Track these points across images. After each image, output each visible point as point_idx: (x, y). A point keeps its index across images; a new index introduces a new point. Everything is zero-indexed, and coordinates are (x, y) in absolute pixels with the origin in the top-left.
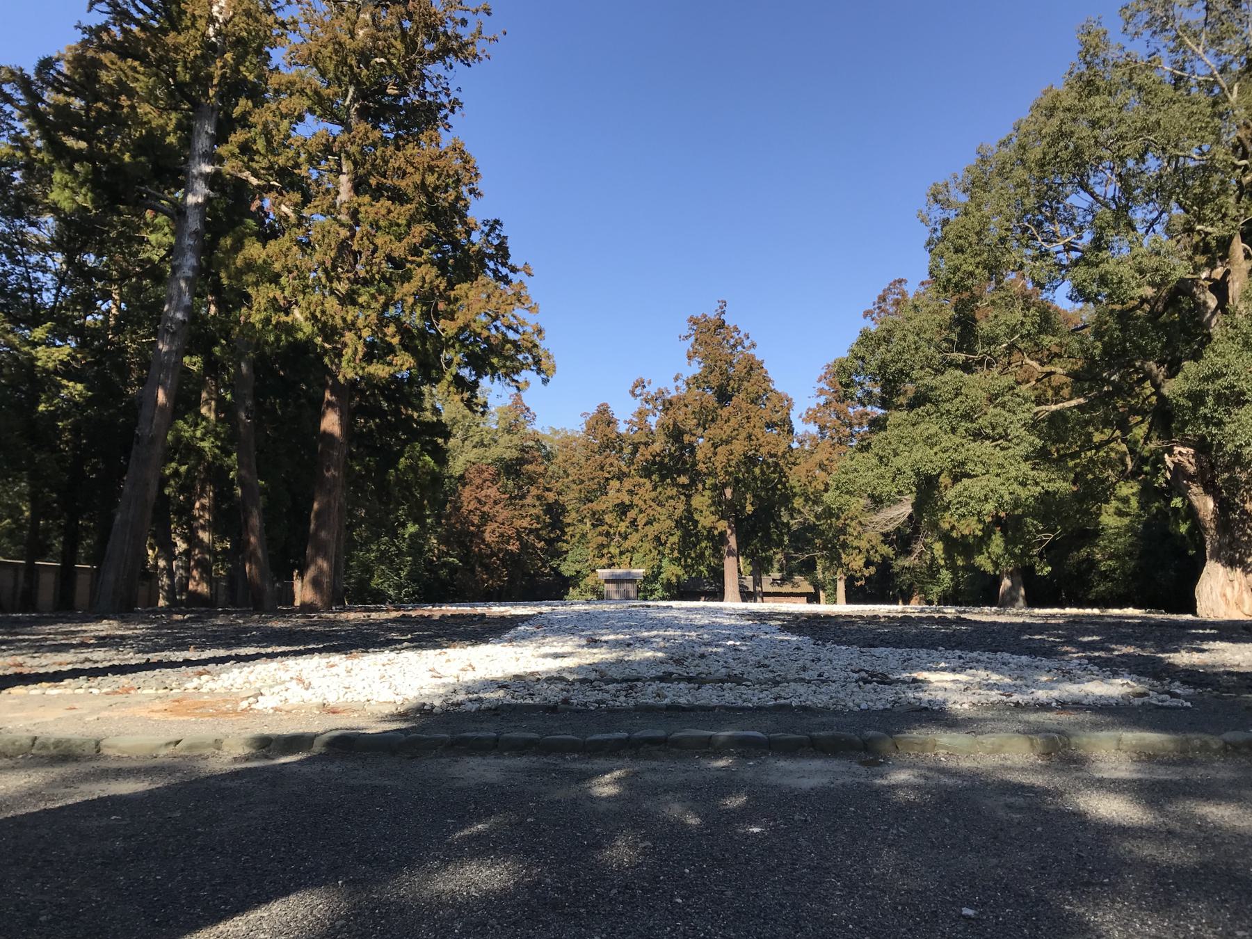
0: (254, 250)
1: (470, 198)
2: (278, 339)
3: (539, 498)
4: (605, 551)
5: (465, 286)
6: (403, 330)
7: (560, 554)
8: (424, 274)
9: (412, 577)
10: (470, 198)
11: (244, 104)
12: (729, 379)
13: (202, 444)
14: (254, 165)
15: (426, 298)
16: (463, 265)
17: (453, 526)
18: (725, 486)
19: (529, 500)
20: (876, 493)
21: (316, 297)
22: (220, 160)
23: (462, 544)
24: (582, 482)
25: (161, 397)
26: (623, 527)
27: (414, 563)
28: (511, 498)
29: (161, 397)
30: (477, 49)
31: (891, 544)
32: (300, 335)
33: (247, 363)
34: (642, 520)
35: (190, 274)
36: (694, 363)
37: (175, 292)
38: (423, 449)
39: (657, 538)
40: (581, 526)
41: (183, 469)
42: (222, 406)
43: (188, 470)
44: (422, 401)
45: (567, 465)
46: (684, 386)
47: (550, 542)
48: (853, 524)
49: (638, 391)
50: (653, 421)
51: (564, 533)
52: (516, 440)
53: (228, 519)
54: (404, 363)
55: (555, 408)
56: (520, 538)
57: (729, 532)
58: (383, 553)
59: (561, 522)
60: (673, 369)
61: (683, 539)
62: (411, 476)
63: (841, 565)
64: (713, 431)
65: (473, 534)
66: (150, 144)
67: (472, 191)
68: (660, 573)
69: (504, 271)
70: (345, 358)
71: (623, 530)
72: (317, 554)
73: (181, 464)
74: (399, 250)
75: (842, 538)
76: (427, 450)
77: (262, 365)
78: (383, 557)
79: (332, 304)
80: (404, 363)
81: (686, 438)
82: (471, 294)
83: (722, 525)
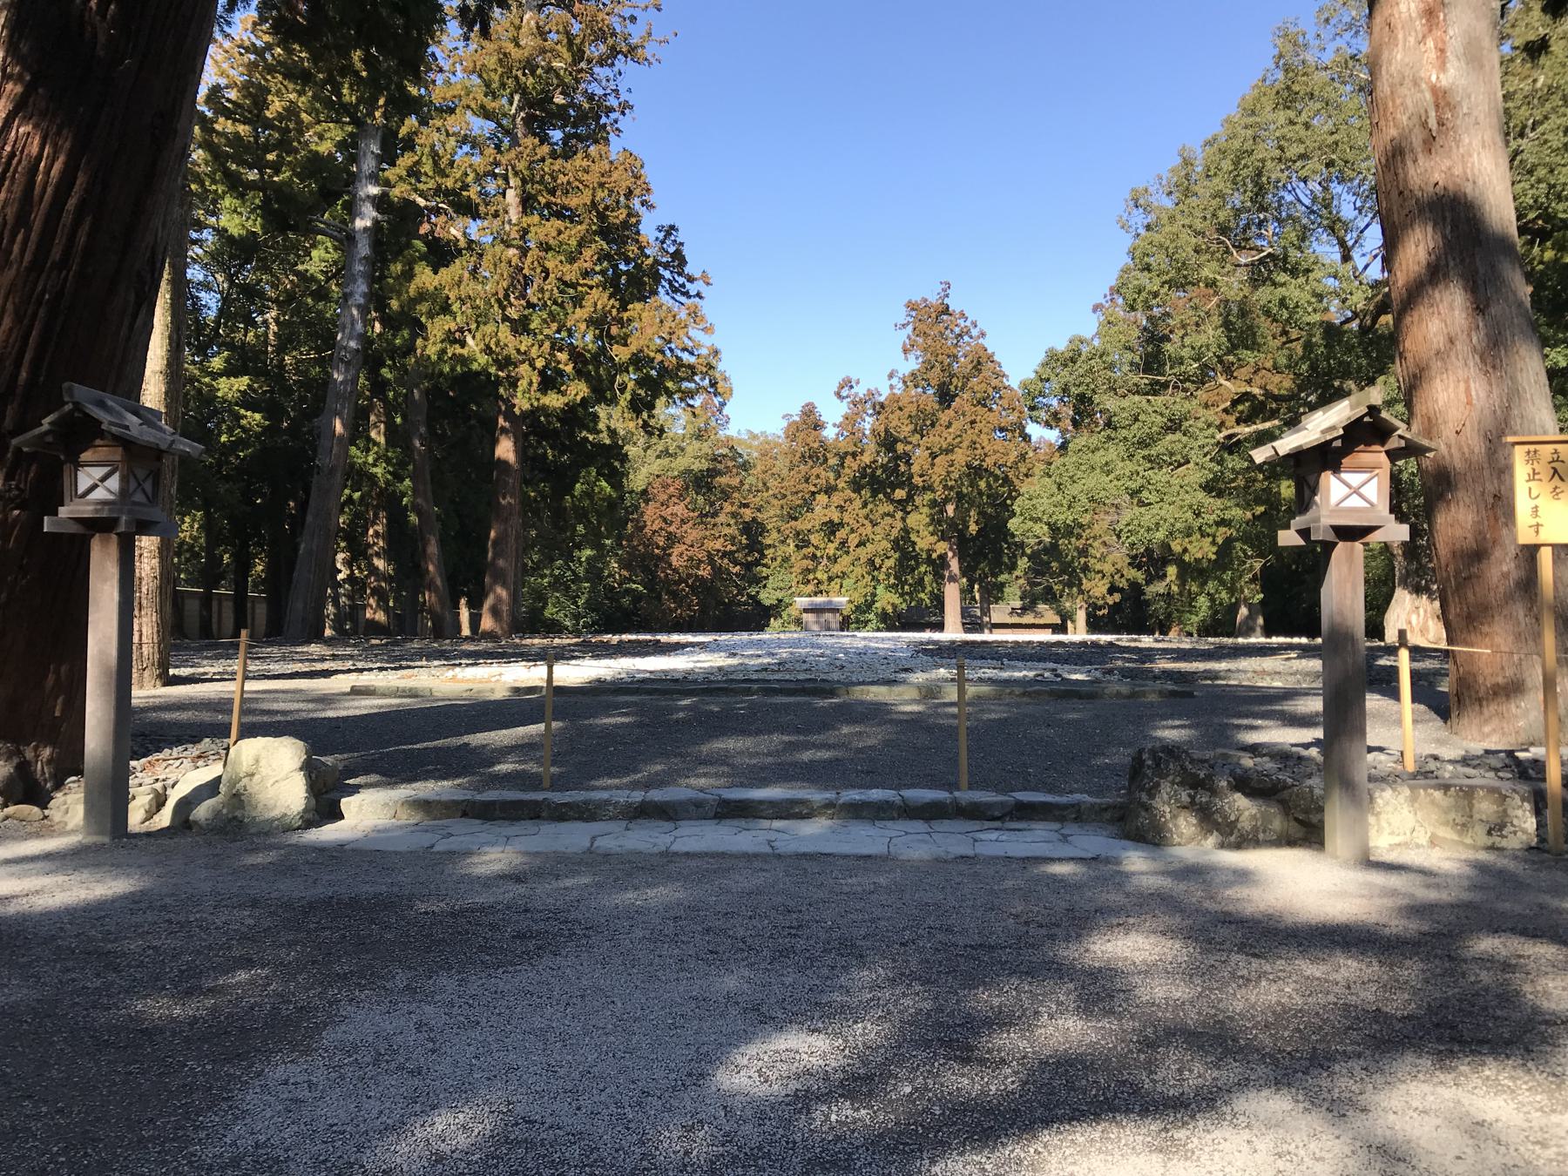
0: (425, 278)
1: (642, 210)
2: (453, 369)
3: (734, 515)
4: (811, 577)
5: (638, 306)
6: (576, 355)
7: (759, 581)
8: (598, 299)
9: (591, 606)
10: (642, 210)
11: (412, 122)
12: (952, 376)
13: (375, 470)
14: (421, 186)
15: (598, 323)
16: (635, 284)
17: (635, 548)
18: (946, 501)
19: (722, 518)
20: (1052, 521)
21: (489, 328)
22: (387, 183)
23: (646, 569)
24: (785, 496)
25: (339, 427)
26: (831, 549)
27: (592, 590)
28: (702, 515)
29: (339, 427)
30: (648, 53)
31: (1139, 568)
32: (475, 366)
33: (420, 391)
34: (853, 540)
35: (362, 301)
36: (911, 357)
37: (348, 321)
38: (598, 474)
39: (871, 562)
40: (783, 548)
41: (357, 495)
42: (392, 433)
43: (362, 497)
44: (596, 424)
45: (767, 477)
46: (901, 385)
47: (748, 566)
48: (1096, 544)
49: (844, 393)
50: (868, 424)
51: (763, 556)
52: (706, 448)
53: (402, 544)
54: (578, 390)
55: (755, 414)
56: (711, 561)
57: (950, 554)
58: (557, 579)
59: (761, 543)
60: (884, 364)
61: (900, 561)
62: (586, 503)
63: (1081, 592)
64: (935, 439)
65: (660, 559)
66: (316, 165)
67: (643, 203)
68: (874, 602)
69: (681, 280)
70: (520, 389)
71: (831, 553)
72: (495, 582)
73: (354, 491)
74: (571, 273)
75: (1083, 560)
76: (603, 475)
77: (434, 393)
78: (557, 583)
79: (505, 332)
80: (578, 390)
81: (900, 447)
82: (644, 315)
83: (942, 547)
